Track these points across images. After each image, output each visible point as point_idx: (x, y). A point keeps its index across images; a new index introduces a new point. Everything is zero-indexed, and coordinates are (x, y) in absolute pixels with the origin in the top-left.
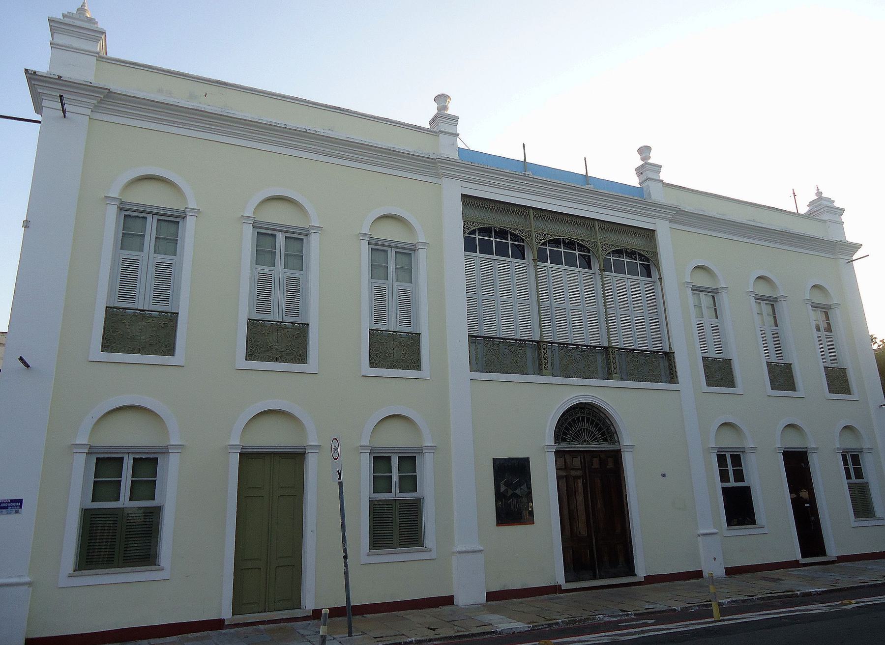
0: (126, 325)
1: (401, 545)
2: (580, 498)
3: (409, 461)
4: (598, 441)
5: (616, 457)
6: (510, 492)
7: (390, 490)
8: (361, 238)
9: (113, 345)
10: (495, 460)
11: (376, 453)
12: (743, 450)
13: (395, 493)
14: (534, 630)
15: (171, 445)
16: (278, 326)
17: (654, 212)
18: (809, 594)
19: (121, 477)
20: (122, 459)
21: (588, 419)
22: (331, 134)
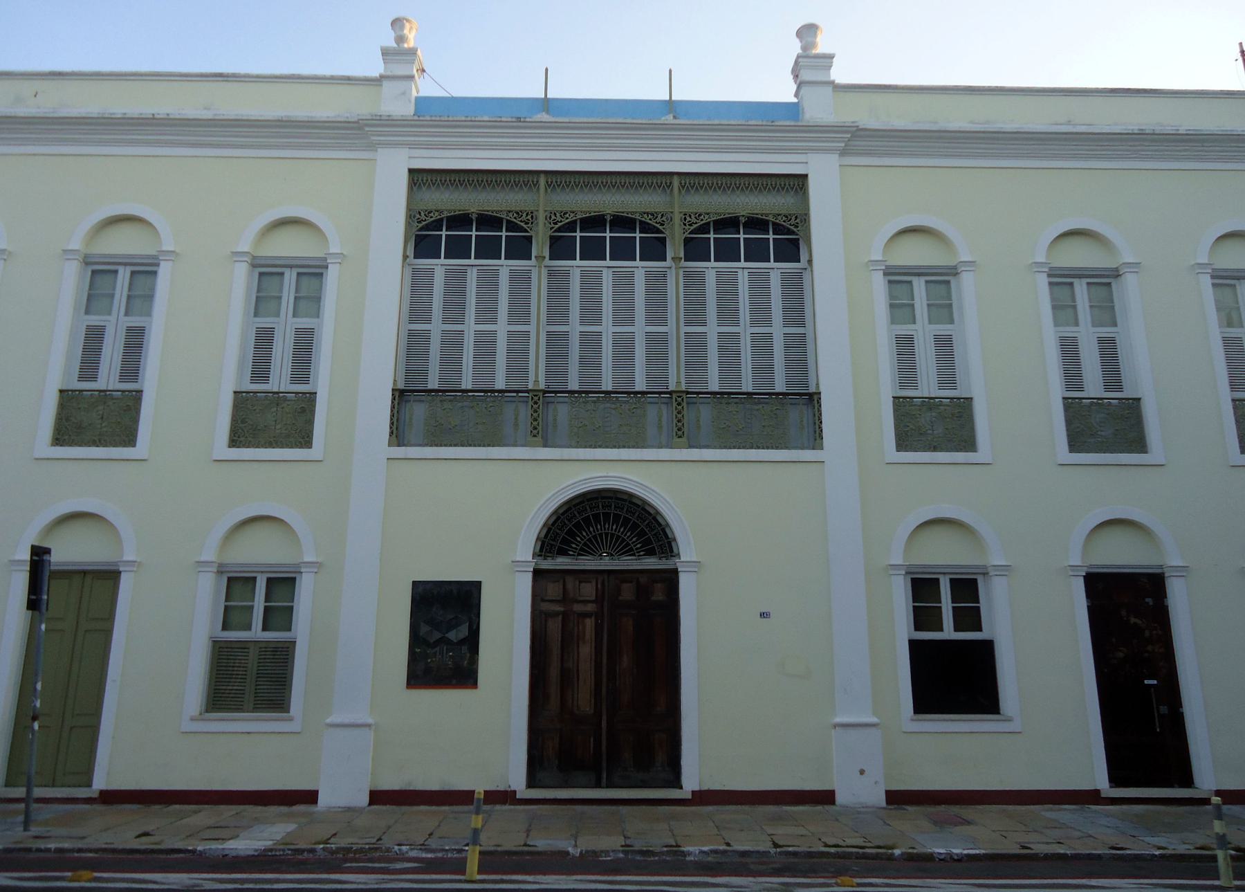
0: (917, 418)
1: (256, 709)
2: (586, 651)
3: (966, 588)
4: (634, 555)
5: (670, 580)
6: (437, 635)
7: (248, 627)
8: (235, 259)
9: (242, 439)
10: (415, 584)
11: (231, 572)
12: (984, 571)
13: (256, 632)
14: (266, 856)
15: (304, 563)
16: (930, 403)
17: (598, 138)
18: (930, 858)
19: (293, 602)
20: (255, 578)
21: (607, 516)
22: (64, 113)
